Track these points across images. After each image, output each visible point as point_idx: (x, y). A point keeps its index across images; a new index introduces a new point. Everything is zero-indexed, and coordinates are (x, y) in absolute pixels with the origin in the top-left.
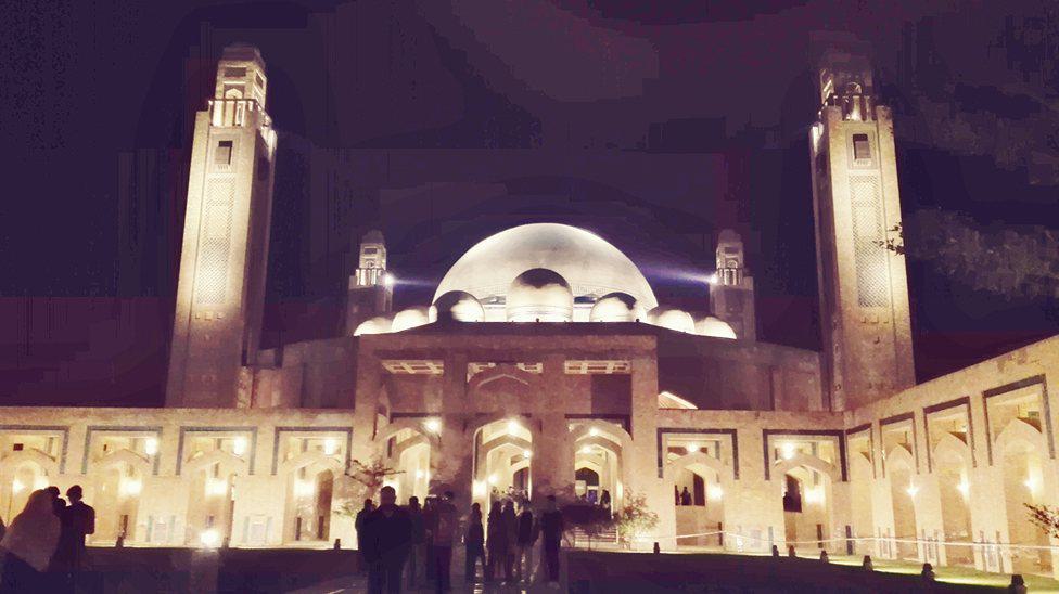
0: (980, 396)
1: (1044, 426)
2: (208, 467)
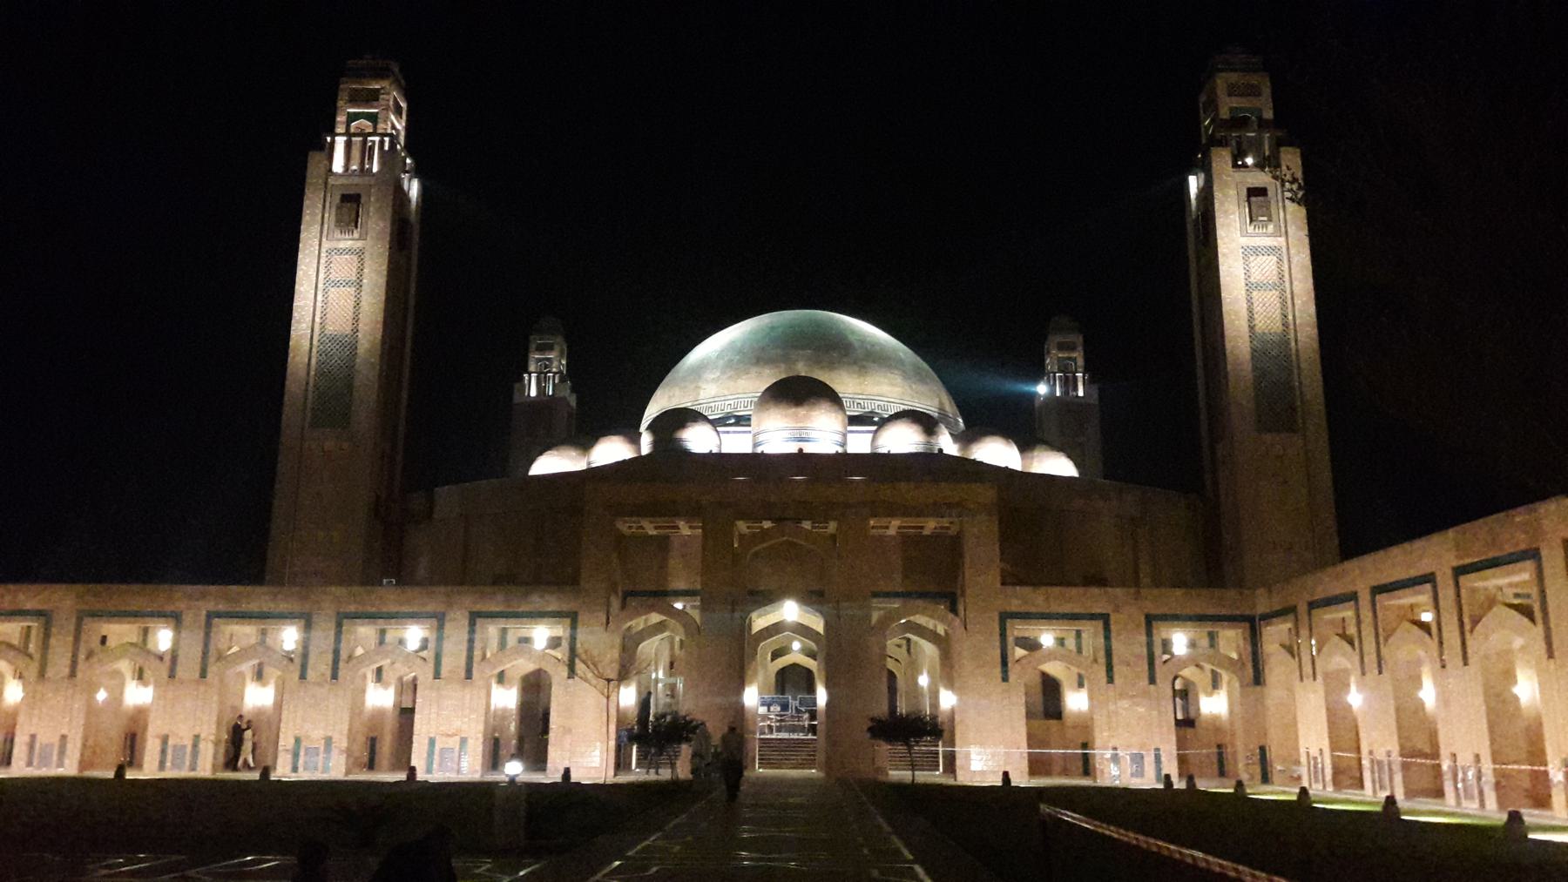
0: (1449, 572)
1: (1538, 615)
2: (247, 667)
